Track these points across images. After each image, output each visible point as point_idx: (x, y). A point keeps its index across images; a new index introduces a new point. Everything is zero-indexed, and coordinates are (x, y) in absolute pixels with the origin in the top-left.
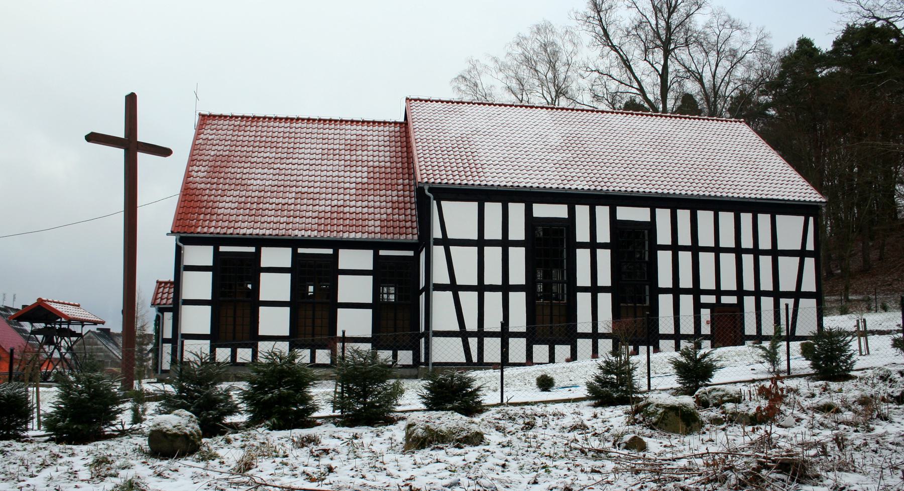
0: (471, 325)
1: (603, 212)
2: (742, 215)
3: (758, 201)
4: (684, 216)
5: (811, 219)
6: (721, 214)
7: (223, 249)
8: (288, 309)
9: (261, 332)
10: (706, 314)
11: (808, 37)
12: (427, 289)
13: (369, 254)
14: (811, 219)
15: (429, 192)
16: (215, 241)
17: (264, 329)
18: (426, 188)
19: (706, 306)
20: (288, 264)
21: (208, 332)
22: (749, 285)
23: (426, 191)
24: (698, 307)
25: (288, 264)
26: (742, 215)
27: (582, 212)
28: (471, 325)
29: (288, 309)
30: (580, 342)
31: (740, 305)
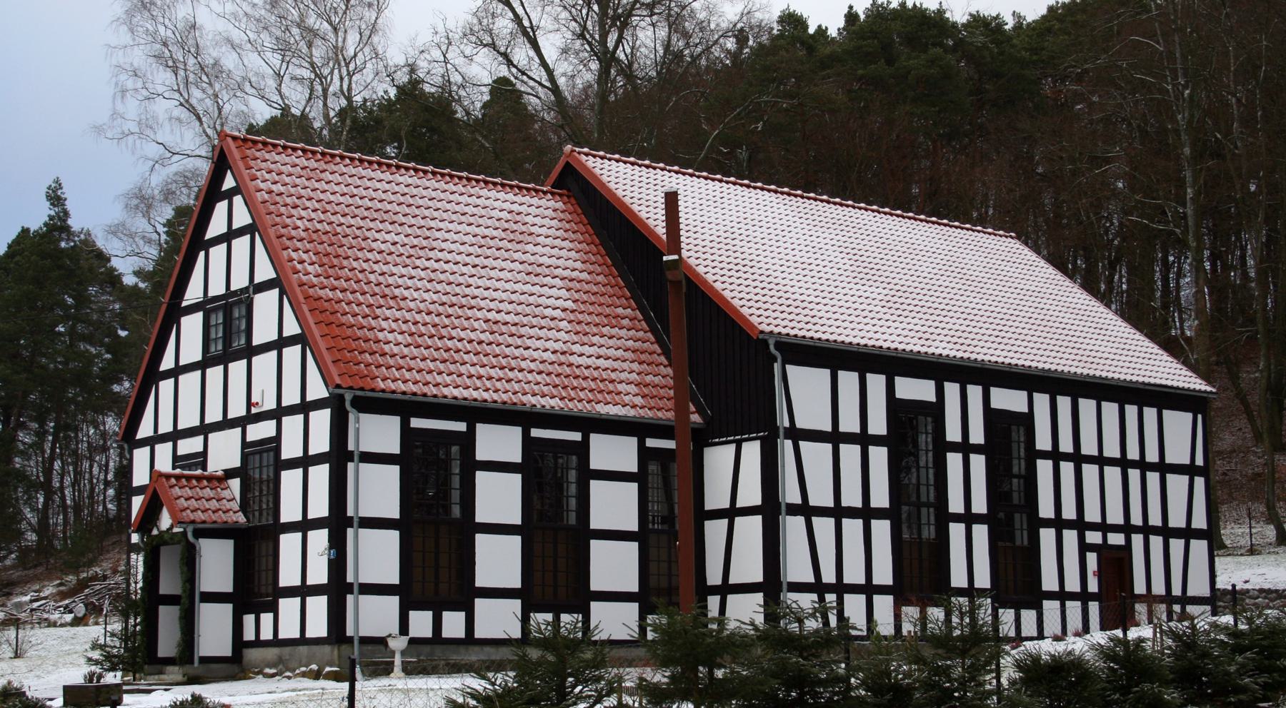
0: (829, 577)
1: (876, 383)
2: (1127, 407)
3: (1147, 387)
4: (1064, 403)
5: (1200, 417)
6: (1104, 404)
7: (416, 423)
8: (1192, 541)
9: (595, 585)
10: (1092, 558)
11: (798, 12)
12: (568, 511)
13: (515, 433)
14: (1200, 417)
15: (776, 348)
16: (403, 407)
17: (598, 582)
18: (771, 342)
19: (1093, 548)
20: (516, 456)
21: (517, 584)
22: (1136, 520)
23: (772, 348)
24: (1084, 548)
25: (516, 456)
26: (1127, 407)
27: (952, 390)
28: (829, 577)
29: (1192, 541)
30: (1047, 604)
31: (1128, 546)
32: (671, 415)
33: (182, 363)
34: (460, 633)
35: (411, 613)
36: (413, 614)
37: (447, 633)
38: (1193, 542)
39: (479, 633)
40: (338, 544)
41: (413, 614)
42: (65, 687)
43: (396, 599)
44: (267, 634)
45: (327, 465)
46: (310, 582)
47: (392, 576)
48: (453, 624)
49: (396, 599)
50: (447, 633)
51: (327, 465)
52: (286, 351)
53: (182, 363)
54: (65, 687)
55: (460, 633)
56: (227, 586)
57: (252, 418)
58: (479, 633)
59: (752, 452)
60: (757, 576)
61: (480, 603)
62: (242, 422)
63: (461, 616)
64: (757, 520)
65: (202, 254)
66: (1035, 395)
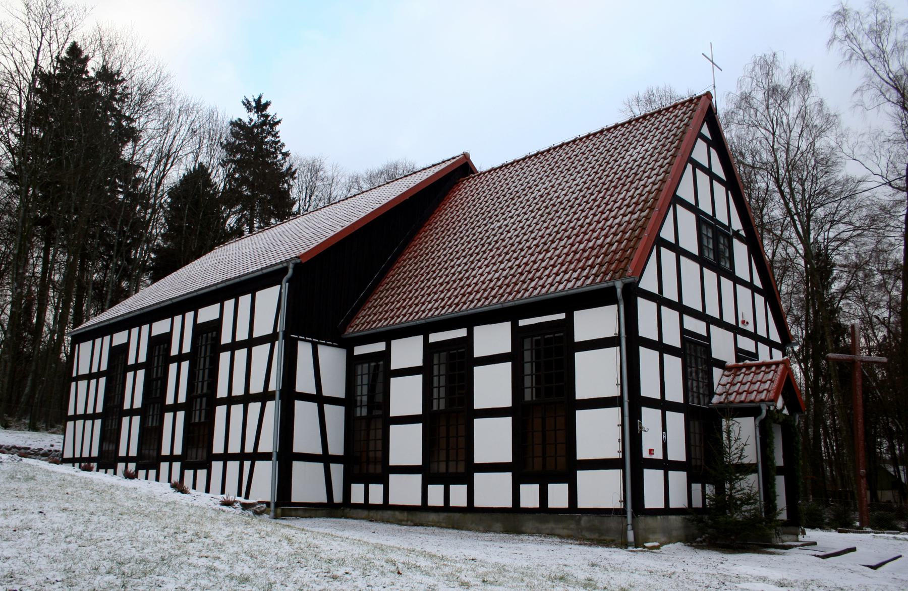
32: (150, 425)
33: (255, 335)
34: (564, 503)
35: (522, 486)
36: (693, 485)
37: (431, 502)
38: (229, 463)
39: (478, 503)
41: (693, 485)
42: (466, 156)
43: (420, 476)
45: (315, 393)
46: (238, 463)
47: (506, 456)
48: (558, 496)
49: (420, 476)
50: (431, 502)
51: (315, 393)
52: (87, 372)
53: (255, 335)
54: (466, 156)
55: (564, 503)
56: (506, 456)
58: (478, 503)
60: (297, 467)
61: (393, 478)
63: (464, 488)
64: (297, 448)
66: (668, 413)
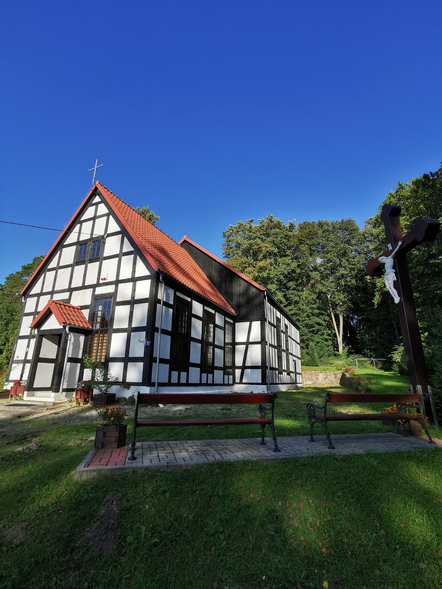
40: (150, 337)
44: (210, 382)
57: (98, 285)
59: (256, 325)
62: (93, 287)
65: (78, 226)
